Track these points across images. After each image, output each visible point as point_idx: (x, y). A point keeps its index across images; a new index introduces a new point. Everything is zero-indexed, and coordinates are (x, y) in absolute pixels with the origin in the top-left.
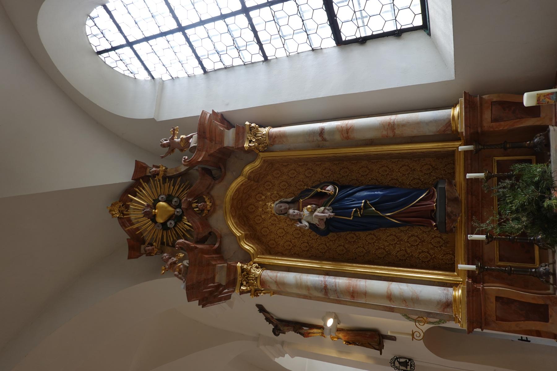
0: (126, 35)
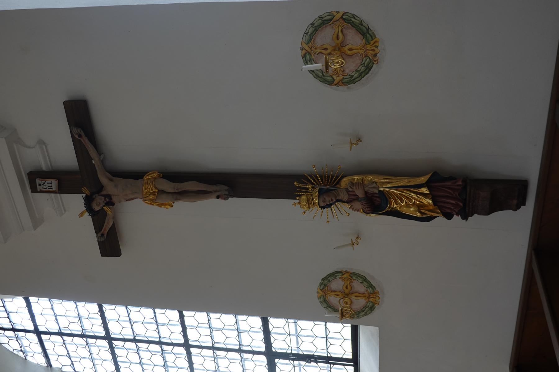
0: (38, 324)
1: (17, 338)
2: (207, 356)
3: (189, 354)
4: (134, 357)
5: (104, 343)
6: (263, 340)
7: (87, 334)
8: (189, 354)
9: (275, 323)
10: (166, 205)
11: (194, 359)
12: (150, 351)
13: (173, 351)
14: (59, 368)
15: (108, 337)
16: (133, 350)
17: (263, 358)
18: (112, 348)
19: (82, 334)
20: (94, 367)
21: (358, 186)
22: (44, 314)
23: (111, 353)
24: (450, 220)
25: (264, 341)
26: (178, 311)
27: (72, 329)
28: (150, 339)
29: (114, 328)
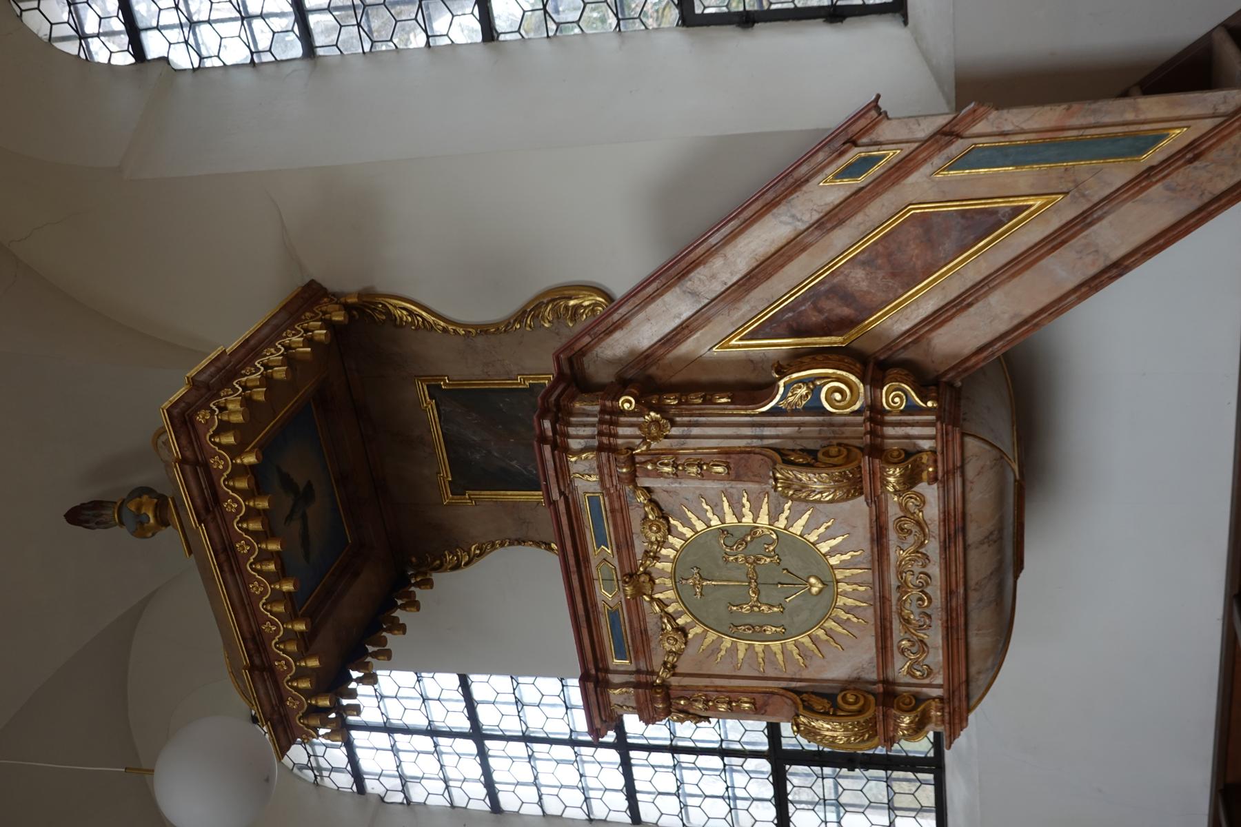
1: (437, 751)
2: (660, 767)
3: (483, 755)
4: (667, 782)
5: (469, 746)
6: (766, 731)
7: (680, 744)
8: (483, 755)
9: (481, 686)
10: (801, 450)
11: (636, 772)
12: (746, 771)
13: (744, 766)
14: (379, 795)
15: (477, 734)
16: (762, 773)
17: (765, 765)
18: (626, 766)
19: (429, 728)
20: (448, 792)
21: (617, 424)
22: (444, 700)
23: (480, 765)
24: (69, 523)
25: (766, 733)
26: (459, 675)
27: (452, 726)
28: (700, 745)
29: (487, 717)
